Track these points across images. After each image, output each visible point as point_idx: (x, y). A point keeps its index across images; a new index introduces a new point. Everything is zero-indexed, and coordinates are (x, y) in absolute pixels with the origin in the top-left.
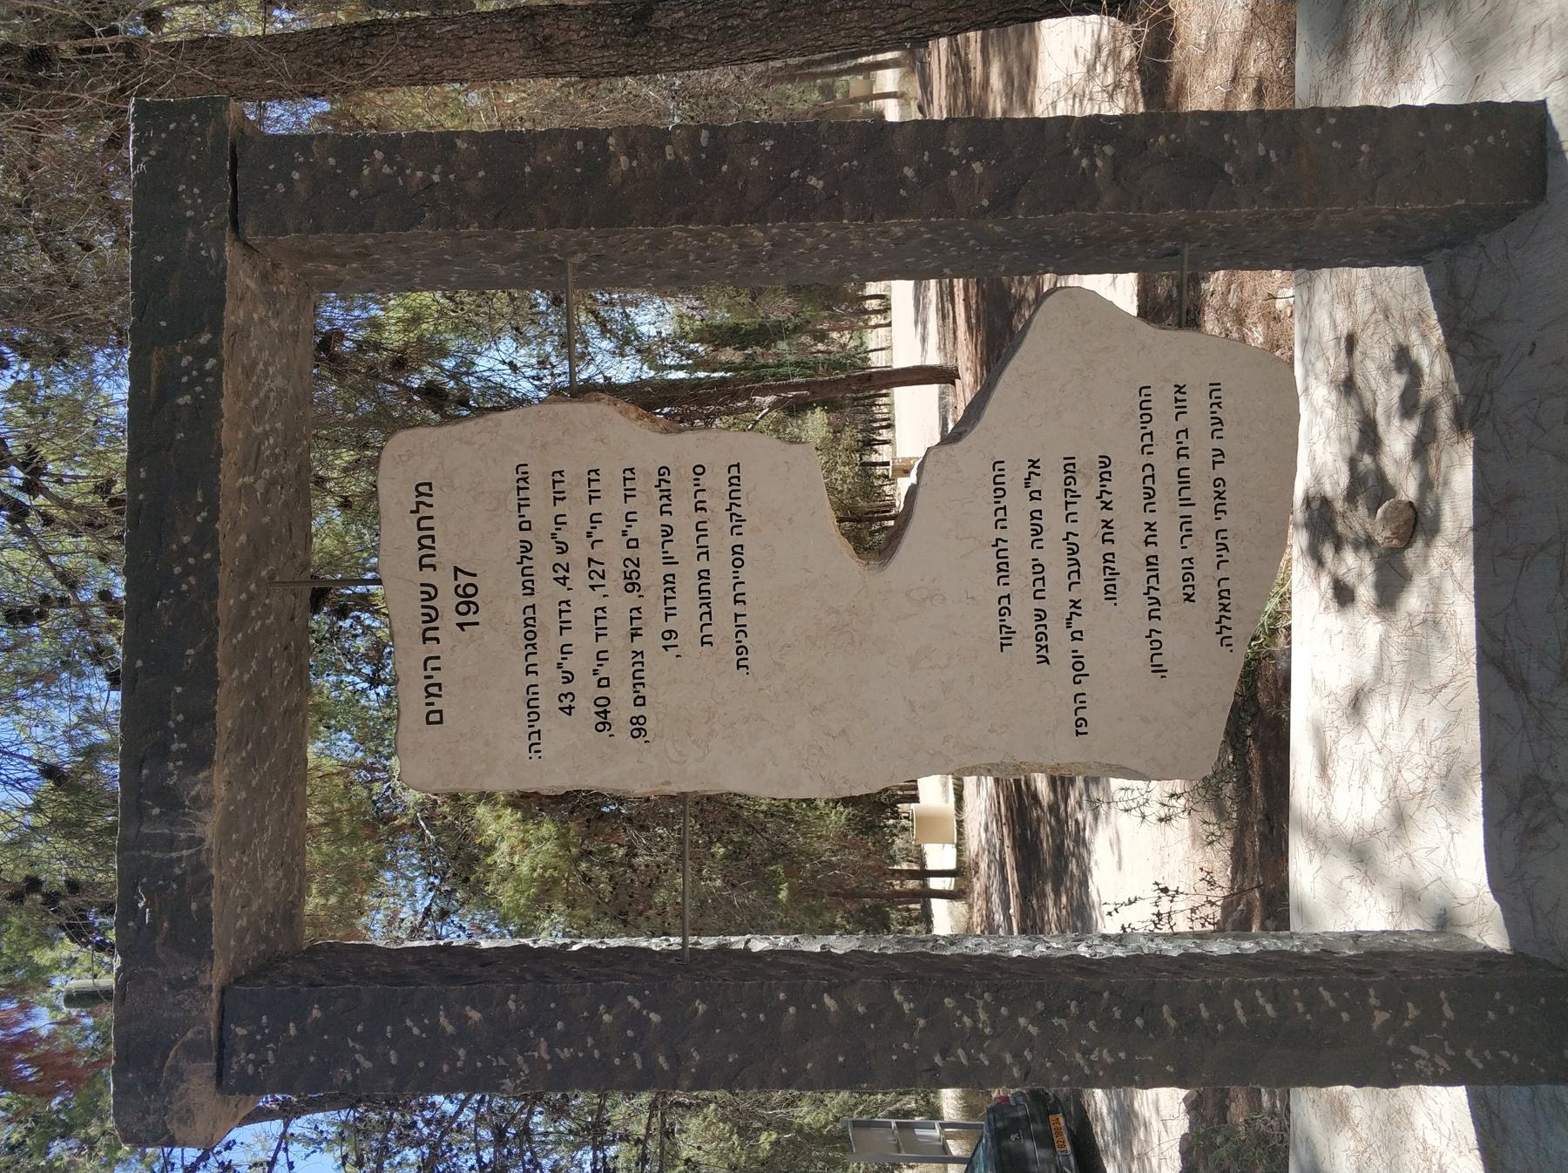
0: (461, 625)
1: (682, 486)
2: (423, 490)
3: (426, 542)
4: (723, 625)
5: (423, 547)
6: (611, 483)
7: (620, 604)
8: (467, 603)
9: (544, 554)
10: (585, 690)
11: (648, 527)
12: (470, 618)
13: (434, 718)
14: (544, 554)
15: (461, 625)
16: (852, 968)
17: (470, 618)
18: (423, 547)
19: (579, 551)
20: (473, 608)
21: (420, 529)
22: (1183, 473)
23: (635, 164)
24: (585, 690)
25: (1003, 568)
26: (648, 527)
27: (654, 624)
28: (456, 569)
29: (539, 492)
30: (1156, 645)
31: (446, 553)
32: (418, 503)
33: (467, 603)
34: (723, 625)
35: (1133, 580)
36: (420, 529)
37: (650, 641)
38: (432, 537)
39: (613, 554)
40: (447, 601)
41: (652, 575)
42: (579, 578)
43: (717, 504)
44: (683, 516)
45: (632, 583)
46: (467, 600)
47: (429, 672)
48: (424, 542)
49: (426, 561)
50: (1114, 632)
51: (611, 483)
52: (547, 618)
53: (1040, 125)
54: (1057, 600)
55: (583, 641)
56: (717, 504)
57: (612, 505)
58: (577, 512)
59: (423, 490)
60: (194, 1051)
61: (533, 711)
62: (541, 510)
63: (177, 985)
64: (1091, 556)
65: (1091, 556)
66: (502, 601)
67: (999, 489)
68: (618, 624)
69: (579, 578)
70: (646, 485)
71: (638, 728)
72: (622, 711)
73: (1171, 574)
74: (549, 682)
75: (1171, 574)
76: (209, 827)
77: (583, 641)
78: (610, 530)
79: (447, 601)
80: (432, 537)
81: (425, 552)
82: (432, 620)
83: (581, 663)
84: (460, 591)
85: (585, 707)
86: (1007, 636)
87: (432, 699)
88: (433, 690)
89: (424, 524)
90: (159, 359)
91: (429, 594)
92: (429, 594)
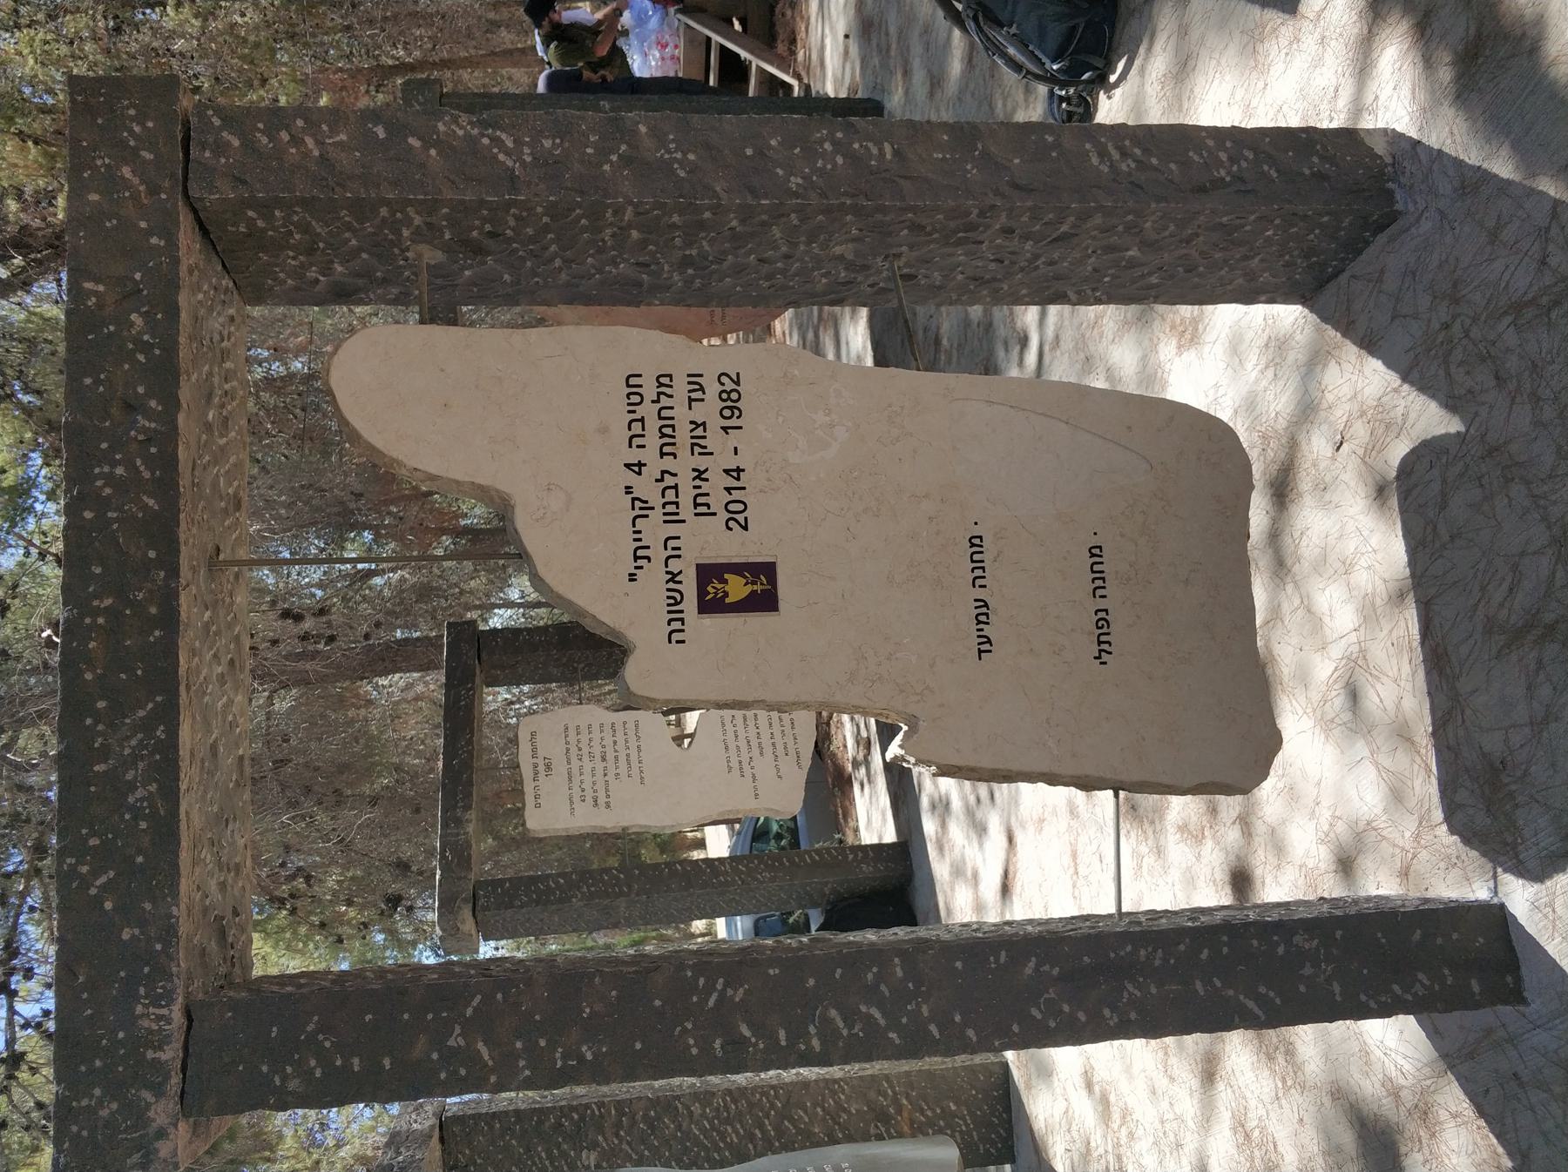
0: (725, 429)
1: (619, 727)
2: (533, 734)
3: (668, 431)
4: (635, 771)
5: (663, 435)
6: (596, 728)
7: (600, 766)
9: (574, 750)
10: (589, 794)
11: (608, 741)
12: (734, 422)
13: (538, 806)
14: (574, 750)
15: (725, 429)
17: (734, 422)
19: (585, 750)
20: (737, 413)
21: (660, 418)
22: (633, 381)
24: (589, 794)
25: (727, 748)
26: (608, 741)
27: (612, 772)
29: (572, 733)
31: (541, 753)
32: (659, 394)
34: (635, 771)
35: (768, 750)
36: (660, 418)
37: (611, 777)
38: (673, 427)
39: (597, 750)
40: (541, 768)
41: (610, 756)
42: (586, 758)
43: (631, 733)
44: (620, 738)
45: (604, 759)
46: (548, 767)
49: (666, 449)
50: (765, 766)
51: (596, 728)
52: (575, 771)
54: (745, 758)
55: (587, 778)
56: (631, 733)
57: (596, 735)
58: (584, 738)
59: (533, 734)
60: (465, 900)
61: (572, 802)
62: (572, 738)
63: (460, 879)
64: (754, 743)
65: (754, 743)
66: (560, 767)
68: (599, 772)
69: (586, 758)
70: (607, 728)
71: (608, 805)
72: (602, 800)
73: (780, 747)
74: (576, 791)
75: (780, 747)
76: (471, 828)
77: (587, 778)
78: (596, 743)
79: (541, 768)
80: (673, 427)
83: (587, 786)
85: (589, 800)
86: (730, 769)
89: (664, 413)
91: (536, 766)
92: (536, 766)
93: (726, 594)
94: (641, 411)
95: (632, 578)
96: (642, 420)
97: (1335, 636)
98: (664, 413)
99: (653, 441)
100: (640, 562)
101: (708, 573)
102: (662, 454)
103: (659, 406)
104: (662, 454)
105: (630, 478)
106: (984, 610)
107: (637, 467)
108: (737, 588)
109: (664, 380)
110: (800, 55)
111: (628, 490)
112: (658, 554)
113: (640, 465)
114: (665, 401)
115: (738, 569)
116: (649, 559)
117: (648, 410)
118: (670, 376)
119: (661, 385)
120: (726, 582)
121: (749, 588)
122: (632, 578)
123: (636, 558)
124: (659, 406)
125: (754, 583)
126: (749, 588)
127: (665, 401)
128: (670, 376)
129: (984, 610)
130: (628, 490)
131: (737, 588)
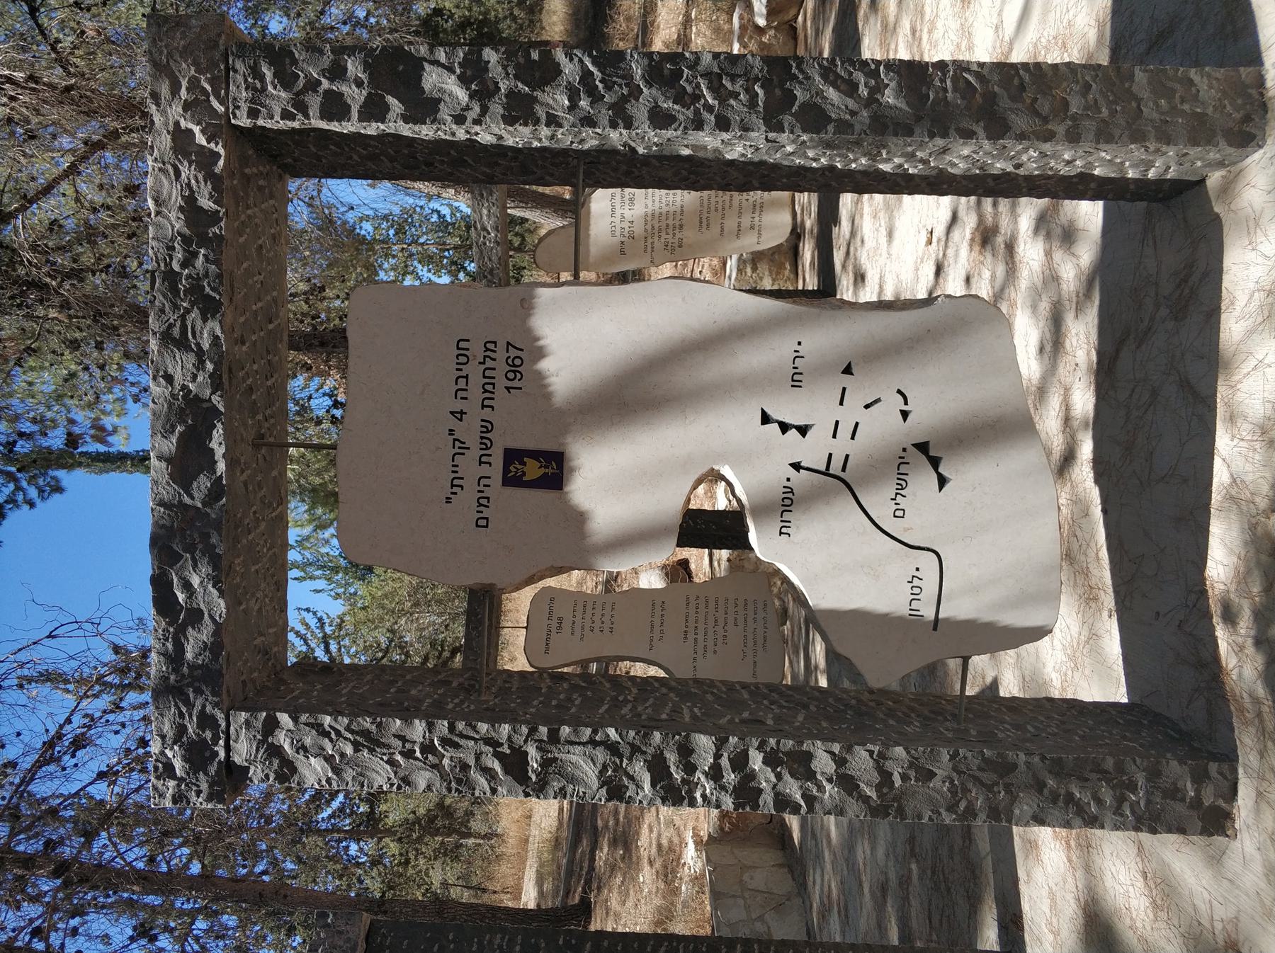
0: (508, 388)
3: (489, 388)
5: (486, 391)
8: (514, 372)
12: (516, 384)
15: (508, 388)
16: (241, 828)
17: (516, 384)
18: (486, 391)
22: (462, 345)
23: (1127, 85)
28: (508, 343)
30: (916, 591)
33: (514, 372)
47: (481, 488)
48: (487, 387)
53: (281, 587)
57: (598, 611)
62: (607, 626)
67: (652, 628)
81: (487, 395)
82: (487, 449)
84: (510, 361)
87: (481, 509)
88: (484, 502)
89: (488, 373)
90: (573, 897)
93: (524, 474)
94: (466, 370)
95: (448, 501)
96: (467, 377)
97: (868, 294)
98: (488, 373)
99: (475, 393)
100: (455, 489)
101: (512, 456)
102: (483, 406)
103: (483, 367)
104: (483, 406)
105: (452, 422)
106: (790, 495)
107: (459, 415)
108: (533, 470)
109: (490, 346)
110: (367, 228)
111: (451, 432)
112: (470, 483)
113: (462, 413)
114: (489, 363)
115: (535, 454)
116: (462, 487)
117: (474, 371)
118: (495, 343)
119: (487, 350)
120: (525, 464)
121: (542, 471)
122: (448, 501)
123: (453, 486)
124: (483, 367)
125: (546, 467)
126: (542, 471)
127: (489, 363)
128: (495, 343)
129: (790, 495)
130: (451, 432)
131: (533, 470)
